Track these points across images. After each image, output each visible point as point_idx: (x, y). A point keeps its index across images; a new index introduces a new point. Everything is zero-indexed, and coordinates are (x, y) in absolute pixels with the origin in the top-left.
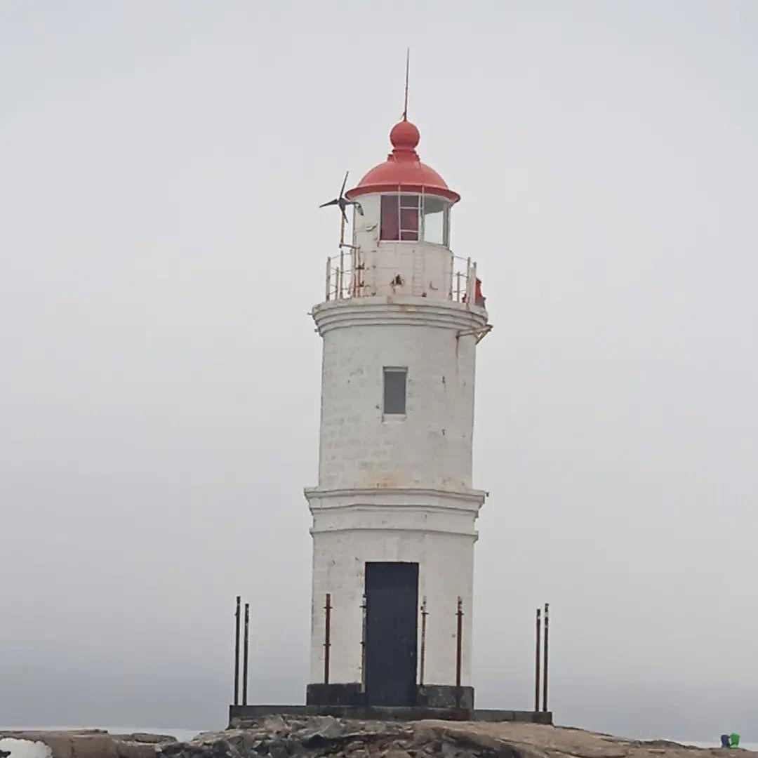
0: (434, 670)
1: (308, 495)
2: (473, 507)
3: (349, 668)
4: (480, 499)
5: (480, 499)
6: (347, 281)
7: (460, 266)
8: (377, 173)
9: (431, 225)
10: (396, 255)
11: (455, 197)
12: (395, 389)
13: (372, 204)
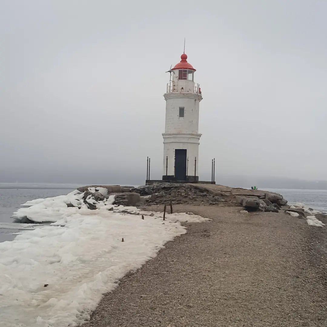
0: (190, 173)
1: (163, 135)
2: (199, 137)
3: (171, 172)
4: (200, 135)
5: (200, 135)
6: (171, 88)
7: (196, 85)
8: (178, 65)
9: (190, 76)
10: (182, 83)
11: (195, 70)
12: (182, 112)
13: (177, 72)
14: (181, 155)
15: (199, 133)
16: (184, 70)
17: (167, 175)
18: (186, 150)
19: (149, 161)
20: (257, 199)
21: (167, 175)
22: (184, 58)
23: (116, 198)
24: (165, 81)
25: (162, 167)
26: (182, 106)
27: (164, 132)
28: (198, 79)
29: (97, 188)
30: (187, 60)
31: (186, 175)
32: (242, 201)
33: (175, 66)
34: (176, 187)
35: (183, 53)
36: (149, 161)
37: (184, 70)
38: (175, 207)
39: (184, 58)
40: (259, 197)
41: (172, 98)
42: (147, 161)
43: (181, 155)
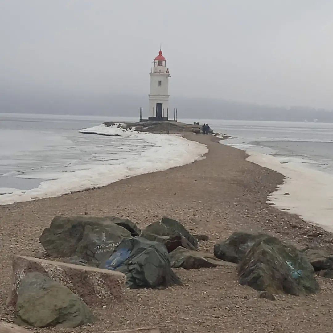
0: (164, 115)
5: (169, 96)
8: (157, 57)
10: (160, 67)
12: (160, 83)
13: (157, 61)
14: (159, 106)
15: (168, 94)
16: (160, 60)
17: (153, 116)
18: (162, 104)
19: (141, 109)
20: (199, 129)
21: (153, 116)
22: (160, 53)
23: (136, 128)
24: (150, 65)
25: (150, 112)
26: (160, 80)
27: (149, 94)
28: (168, 64)
29: (121, 124)
30: (162, 54)
31: (163, 117)
32: (193, 130)
33: (156, 58)
34: (160, 124)
35: (160, 51)
36: (141, 109)
37: (160, 60)
38: (169, 132)
39: (160, 53)
40: (199, 128)
41: (219, 126)
42: (177, 117)
43: (159, 106)
